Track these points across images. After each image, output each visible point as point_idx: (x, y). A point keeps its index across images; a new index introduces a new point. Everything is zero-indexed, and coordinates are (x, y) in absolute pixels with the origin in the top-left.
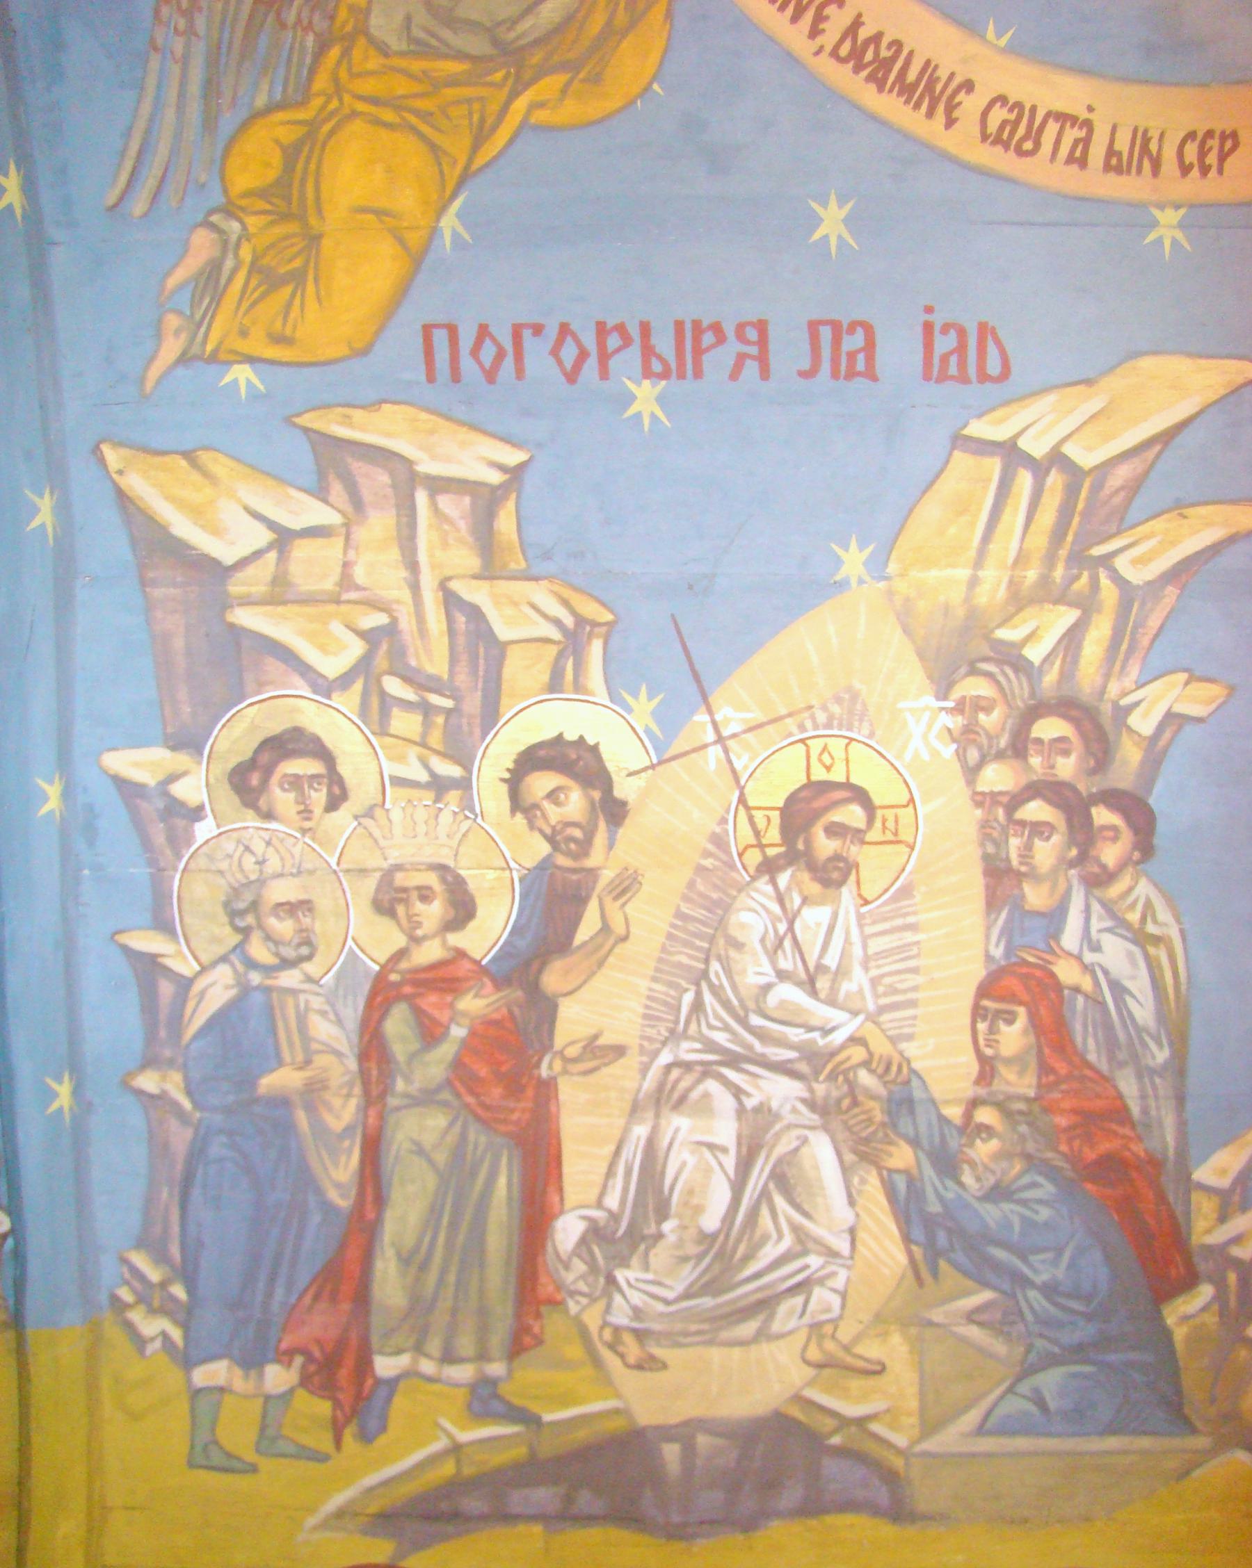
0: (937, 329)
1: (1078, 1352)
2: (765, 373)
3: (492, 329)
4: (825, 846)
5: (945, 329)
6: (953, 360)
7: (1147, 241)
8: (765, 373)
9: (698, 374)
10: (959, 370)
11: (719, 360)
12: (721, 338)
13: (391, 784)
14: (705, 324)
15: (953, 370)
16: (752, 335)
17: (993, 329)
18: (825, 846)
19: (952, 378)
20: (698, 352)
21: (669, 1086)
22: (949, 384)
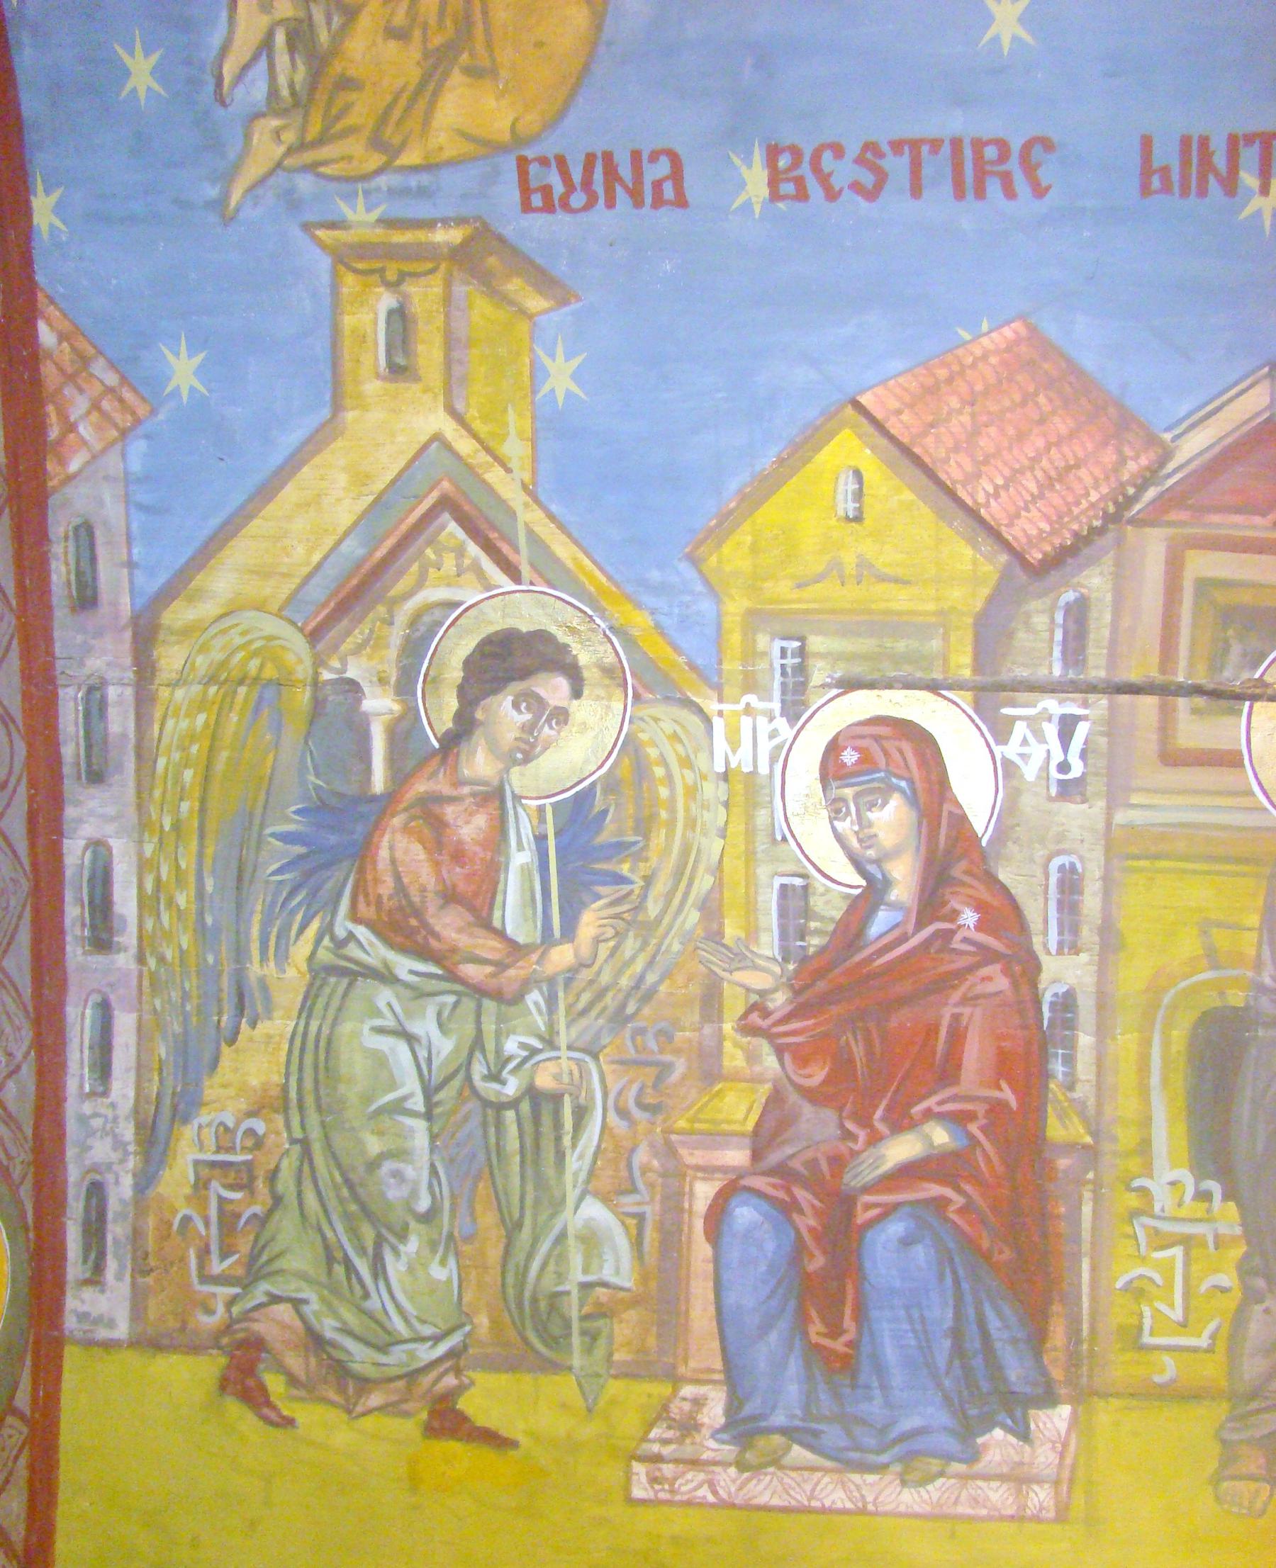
0: (645, 156)
5: (654, 157)
13: (1240, 753)
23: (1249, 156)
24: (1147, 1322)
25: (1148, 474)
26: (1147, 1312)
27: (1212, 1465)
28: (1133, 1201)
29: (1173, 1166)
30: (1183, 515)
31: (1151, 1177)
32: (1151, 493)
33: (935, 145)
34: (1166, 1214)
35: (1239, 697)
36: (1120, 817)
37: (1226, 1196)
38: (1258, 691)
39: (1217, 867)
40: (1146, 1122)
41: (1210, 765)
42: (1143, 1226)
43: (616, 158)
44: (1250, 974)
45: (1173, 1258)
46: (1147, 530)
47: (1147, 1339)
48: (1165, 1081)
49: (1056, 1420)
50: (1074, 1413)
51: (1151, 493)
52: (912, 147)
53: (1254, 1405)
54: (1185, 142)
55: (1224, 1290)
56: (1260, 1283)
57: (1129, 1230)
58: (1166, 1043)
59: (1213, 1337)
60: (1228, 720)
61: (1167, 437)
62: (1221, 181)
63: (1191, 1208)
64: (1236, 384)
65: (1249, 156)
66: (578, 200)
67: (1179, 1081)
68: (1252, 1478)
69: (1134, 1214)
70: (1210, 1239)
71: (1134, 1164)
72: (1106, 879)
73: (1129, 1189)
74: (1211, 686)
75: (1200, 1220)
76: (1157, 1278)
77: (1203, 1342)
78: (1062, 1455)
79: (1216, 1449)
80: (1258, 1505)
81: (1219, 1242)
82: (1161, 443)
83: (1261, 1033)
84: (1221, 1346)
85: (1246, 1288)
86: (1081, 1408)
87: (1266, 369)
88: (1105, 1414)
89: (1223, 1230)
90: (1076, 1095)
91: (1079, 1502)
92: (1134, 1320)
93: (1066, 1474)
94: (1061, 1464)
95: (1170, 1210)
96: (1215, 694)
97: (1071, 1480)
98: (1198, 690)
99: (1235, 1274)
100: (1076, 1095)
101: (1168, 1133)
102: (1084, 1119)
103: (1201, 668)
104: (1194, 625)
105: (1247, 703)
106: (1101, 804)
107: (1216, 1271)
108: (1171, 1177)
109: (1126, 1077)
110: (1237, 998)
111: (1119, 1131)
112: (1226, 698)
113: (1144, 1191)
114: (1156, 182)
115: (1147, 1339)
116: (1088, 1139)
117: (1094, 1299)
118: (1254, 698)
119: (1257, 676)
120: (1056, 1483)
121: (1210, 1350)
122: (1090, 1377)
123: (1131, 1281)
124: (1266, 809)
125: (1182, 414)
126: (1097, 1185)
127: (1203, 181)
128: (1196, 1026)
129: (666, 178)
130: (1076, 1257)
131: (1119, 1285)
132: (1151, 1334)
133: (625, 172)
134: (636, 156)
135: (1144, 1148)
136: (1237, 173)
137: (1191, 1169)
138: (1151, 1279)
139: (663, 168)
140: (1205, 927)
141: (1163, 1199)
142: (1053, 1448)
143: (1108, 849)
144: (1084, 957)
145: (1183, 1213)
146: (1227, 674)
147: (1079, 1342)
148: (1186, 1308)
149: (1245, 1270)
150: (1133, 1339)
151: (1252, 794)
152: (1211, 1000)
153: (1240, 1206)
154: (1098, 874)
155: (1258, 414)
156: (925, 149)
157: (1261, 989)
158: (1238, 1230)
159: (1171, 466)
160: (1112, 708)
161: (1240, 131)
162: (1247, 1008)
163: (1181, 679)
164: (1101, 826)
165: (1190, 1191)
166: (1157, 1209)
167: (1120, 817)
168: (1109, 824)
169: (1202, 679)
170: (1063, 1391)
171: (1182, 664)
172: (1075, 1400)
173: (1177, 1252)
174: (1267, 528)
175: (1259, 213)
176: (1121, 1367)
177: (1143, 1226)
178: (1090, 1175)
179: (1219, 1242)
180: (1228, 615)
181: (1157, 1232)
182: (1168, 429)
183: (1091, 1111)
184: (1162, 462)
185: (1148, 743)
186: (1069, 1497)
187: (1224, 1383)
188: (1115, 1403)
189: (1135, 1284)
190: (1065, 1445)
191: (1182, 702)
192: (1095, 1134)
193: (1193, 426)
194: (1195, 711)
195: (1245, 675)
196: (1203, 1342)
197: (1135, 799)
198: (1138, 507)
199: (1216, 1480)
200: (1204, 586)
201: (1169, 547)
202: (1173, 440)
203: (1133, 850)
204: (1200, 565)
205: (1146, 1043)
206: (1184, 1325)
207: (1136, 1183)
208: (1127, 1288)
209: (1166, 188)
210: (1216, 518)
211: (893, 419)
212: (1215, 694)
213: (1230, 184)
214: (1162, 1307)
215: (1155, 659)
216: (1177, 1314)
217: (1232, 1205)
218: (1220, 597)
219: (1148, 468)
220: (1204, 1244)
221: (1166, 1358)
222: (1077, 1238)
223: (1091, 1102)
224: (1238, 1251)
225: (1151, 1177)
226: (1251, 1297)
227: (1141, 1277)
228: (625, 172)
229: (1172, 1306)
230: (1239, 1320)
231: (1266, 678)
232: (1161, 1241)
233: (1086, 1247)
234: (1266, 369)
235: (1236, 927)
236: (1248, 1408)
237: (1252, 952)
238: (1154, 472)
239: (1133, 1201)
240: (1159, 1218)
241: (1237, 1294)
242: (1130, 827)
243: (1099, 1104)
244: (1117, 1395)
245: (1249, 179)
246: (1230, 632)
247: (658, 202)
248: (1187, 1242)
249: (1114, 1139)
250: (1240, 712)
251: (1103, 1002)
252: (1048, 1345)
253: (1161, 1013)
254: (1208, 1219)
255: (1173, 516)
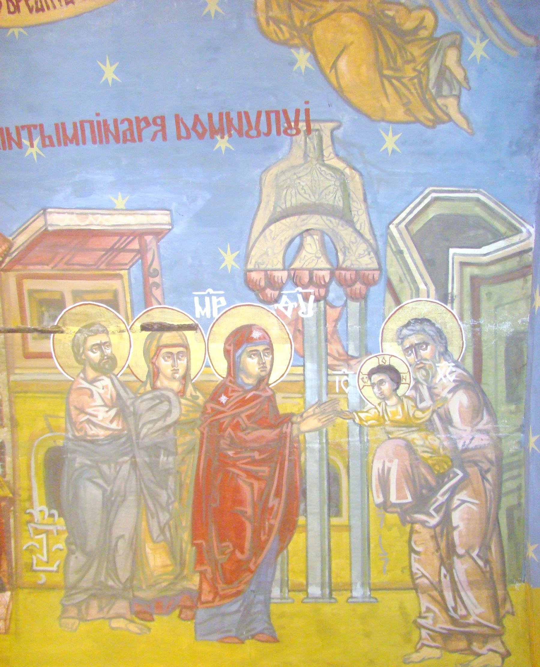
0: (119, 122)
1: (431, 583)
2: (165, 138)
3: (200, 117)
4: (95, 356)
5: (123, 122)
6: (128, 133)
7: (478, 63)
8: (165, 138)
9: (140, 140)
10: (131, 137)
11: (148, 133)
12: (148, 124)
13: (51, 353)
14: (141, 118)
15: (129, 137)
16: (159, 121)
17: (182, 118)
18: (95, 356)
19: (48, 146)
20: (140, 132)
21: (411, 474)
22: (128, 143)
23: (24, 133)
24: (35, 562)
25: (6, 253)
26: (34, 558)
27: (59, 612)
28: (27, 517)
29: (41, 504)
30: (20, 267)
31: (33, 508)
32: (7, 260)
33: (35, 127)
34: (39, 522)
35: (51, 332)
36: (12, 378)
37: (60, 516)
38: (57, 330)
39: (48, 395)
40: (30, 489)
41: (41, 358)
42: (32, 527)
43: (109, 123)
44: (64, 434)
45: (42, 538)
46: (8, 273)
47: (35, 568)
48: (37, 474)
49: (5, 597)
50: (12, 594)
51: (7, 260)
52: (29, 128)
53: (74, 591)
54: (57, 126)
55: (61, 550)
56: (73, 547)
57: (26, 528)
58: (36, 461)
59: (58, 566)
60: (46, 341)
61: (11, 238)
62: (16, 144)
63: (48, 520)
64: (32, 217)
65: (24, 133)
66: (253, 133)
67: (41, 474)
68: (73, 618)
69: (28, 522)
70: (55, 532)
71: (27, 504)
72: (10, 401)
73: (26, 513)
74: (40, 329)
75: (51, 525)
76: (38, 546)
77: (55, 568)
78: (7, 609)
79: (60, 607)
80: (75, 627)
81: (58, 532)
82: (8, 241)
83: (69, 455)
84: (61, 570)
85: (69, 549)
86: (14, 593)
87: (42, 211)
88: (22, 595)
89: (60, 528)
90: (6, 479)
91: (13, 627)
92: (30, 561)
93: (8, 617)
94: (7, 613)
95: (41, 521)
96: (42, 332)
97: (10, 619)
98: (36, 330)
99: (64, 544)
100: (6, 479)
101: (38, 493)
102: (10, 488)
103: (36, 322)
104: (31, 306)
105: (52, 335)
106: (5, 373)
107: (58, 543)
108: (40, 508)
109: (23, 472)
110: (60, 443)
111: (21, 492)
112: (44, 332)
113: (31, 514)
114: (47, 143)
115: (35, 568)
116: (11, 495)
117: (16, 553)
118: (55, 332)
119: (56, 324)
120: (5, 620)
121: (57, 571)
122: (16, 581)
123: (28, 547)
124: (62, 373)
125: (15, 229)
126: (15, 512)
127: (107, 138)
128: (46, 453)
129: (127, 130)
130: (10, 538)
131: (25, 548)
132: (37, 565)
133: (112, 128)
134: (115, 121)
135: (30, 498)
136: (21, 140)
137: (47, 506)
138: (35, 546)
139: (126, 125)
140: (46, 417)
141: (38, 517)
142: (4, 607)
143: (9, 389)
144: (6, 429)
145: (45, 522)
146: (45, 324)
147: (12, 569)
148: (48, 557)
149: (68, 542)
150: (30, 567)
151: (57, 368)
152: (51, 444)
153: (65, 519)
154: (6, 399)
155: (41, 228)
156: (32, 128)
157: (68, 439)
158: (65, 528)
159: (13, 249)
160: (5, 338)
161: (19, 125)
162: (64, 447)
163: (29, 327)
164: (6, 381)
165: (47, 514)
166: (36, 520)
167: (12, 378)
168: (9, 381)
169: (37, 326)
170: (8, 587)
171: (29, 321)
172: (11, 590)
173: (44, 536)
174: (49, 270)
175: (31, 154)
176: (27, 577)
177: (32, 527)
178: (12, 508)
179: (58, 532)
180: (41, 302)
181: (36, 529)
182: (10, 236)
183: (12, 485)
184: (10, 248)
185: (18, 350)
186: (9, 625)
187: (63, 583)
188: (26, 591)
189: (30, 548)
190: (8, 606)
191: (30, 335)
192: (14, 493)
193: (18, 235)
194: (35, 339)
195: (51, 324)
196: (55, 568)
197: (17, 371)
198: (4, 265)
199: (61, 617)
200: (32, 292)
201: (16, 279)
202: (13, 239)
203: (18, 390)
204: (29, 285)
205: (29, 459)
206: (47, 562)
207: (28, 511)
208: (28, 549)
209: (52, 145)
210: (31, 267)
211: (353, 239)
212: (42, 332)
213: (20, 145)
214: (39, 556)
215: (19, 319)
216: (45, 558)
217: (62, 519)
218: (37, 296)
219: (5, 250)
220: (53, 533)
221: (42, 575)
222: (9, 531)
223: (12, 482)
224: (66, 535)
225: (33, 508)
226: (71, 552)
227: (32, 545)
228: (112, 128)
229: (43, 555)
230: (67, 560)
231: (59, 325)
232: (38, 532)
233: (12, 535)
234: (42, 211)
235: (57, 417)
236: (72, 592)
237: (63, 426)
238: (8, 252)
239: (27, 517)
240: (36, 523)
241: (65, 551)
242: (16, 381)
243: (14, 483)
244: (26, 588)
245: (26, 142)
246: (43, 309)
247: (125, 141)
248: (47, 532)
249: (20, 495)
250: (49, 338)
251: (14, 446)
252: (2, 570)
253: (34, 449)
254: (54, 524)
255: (16, 267)
